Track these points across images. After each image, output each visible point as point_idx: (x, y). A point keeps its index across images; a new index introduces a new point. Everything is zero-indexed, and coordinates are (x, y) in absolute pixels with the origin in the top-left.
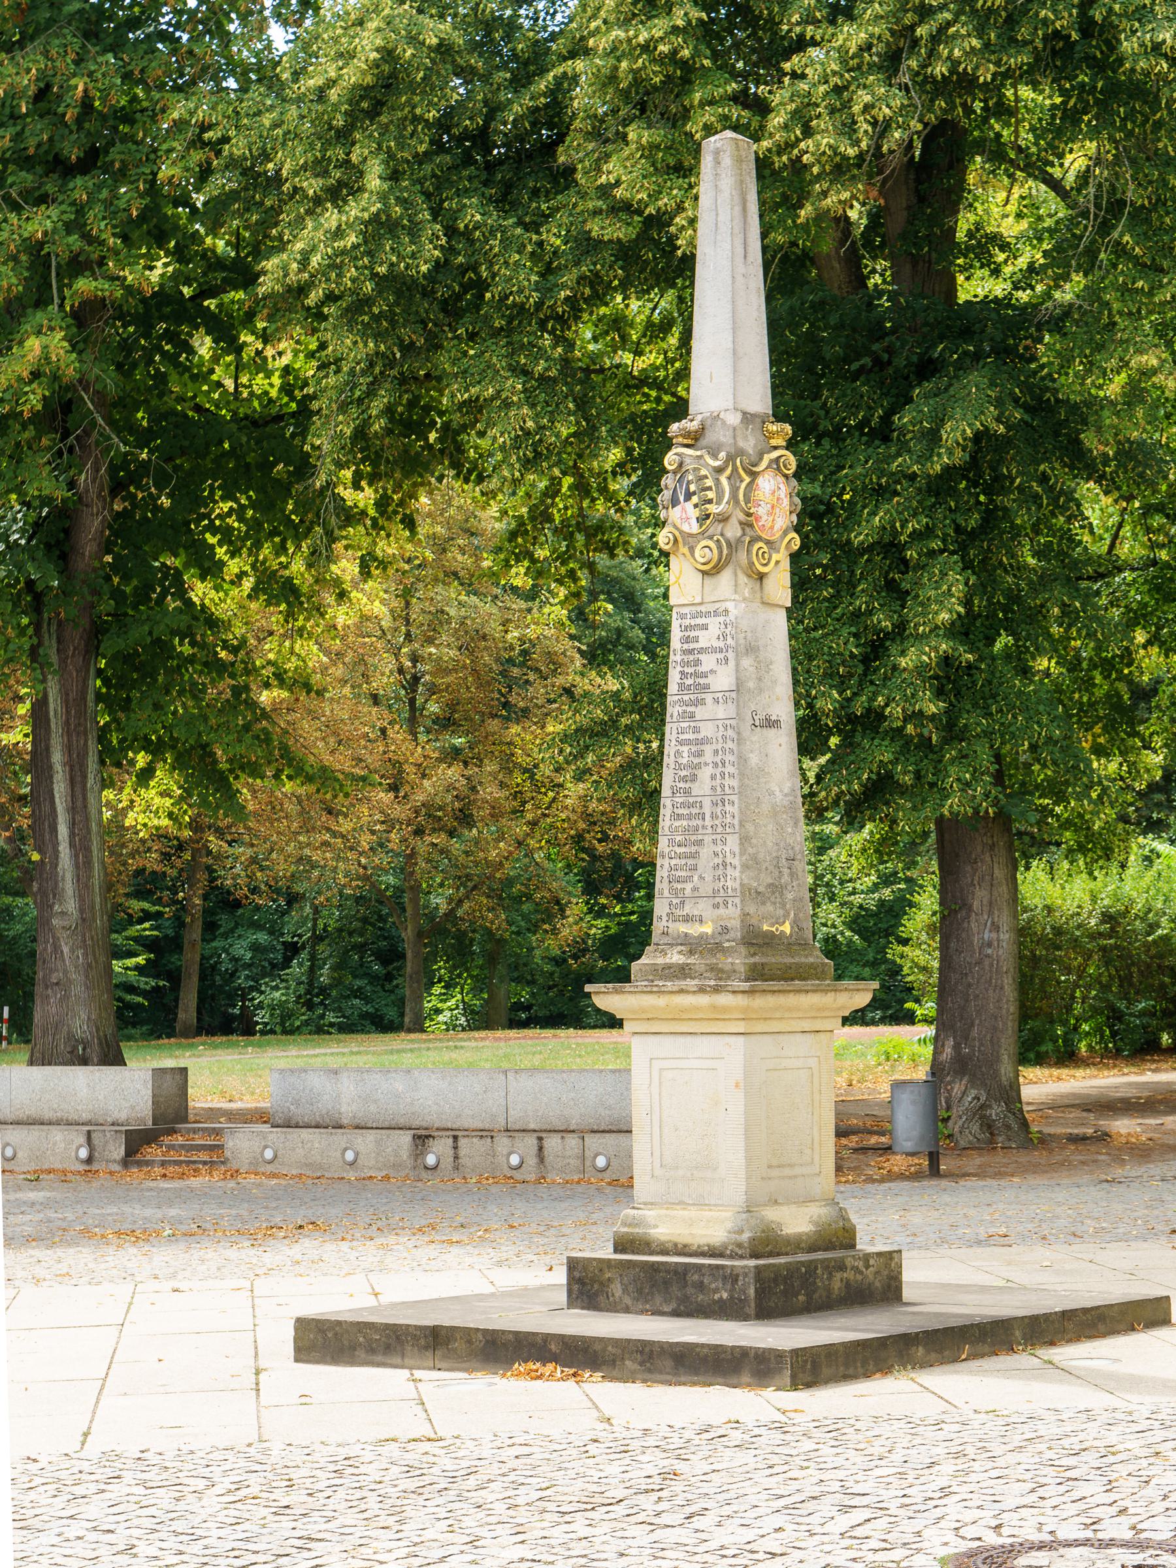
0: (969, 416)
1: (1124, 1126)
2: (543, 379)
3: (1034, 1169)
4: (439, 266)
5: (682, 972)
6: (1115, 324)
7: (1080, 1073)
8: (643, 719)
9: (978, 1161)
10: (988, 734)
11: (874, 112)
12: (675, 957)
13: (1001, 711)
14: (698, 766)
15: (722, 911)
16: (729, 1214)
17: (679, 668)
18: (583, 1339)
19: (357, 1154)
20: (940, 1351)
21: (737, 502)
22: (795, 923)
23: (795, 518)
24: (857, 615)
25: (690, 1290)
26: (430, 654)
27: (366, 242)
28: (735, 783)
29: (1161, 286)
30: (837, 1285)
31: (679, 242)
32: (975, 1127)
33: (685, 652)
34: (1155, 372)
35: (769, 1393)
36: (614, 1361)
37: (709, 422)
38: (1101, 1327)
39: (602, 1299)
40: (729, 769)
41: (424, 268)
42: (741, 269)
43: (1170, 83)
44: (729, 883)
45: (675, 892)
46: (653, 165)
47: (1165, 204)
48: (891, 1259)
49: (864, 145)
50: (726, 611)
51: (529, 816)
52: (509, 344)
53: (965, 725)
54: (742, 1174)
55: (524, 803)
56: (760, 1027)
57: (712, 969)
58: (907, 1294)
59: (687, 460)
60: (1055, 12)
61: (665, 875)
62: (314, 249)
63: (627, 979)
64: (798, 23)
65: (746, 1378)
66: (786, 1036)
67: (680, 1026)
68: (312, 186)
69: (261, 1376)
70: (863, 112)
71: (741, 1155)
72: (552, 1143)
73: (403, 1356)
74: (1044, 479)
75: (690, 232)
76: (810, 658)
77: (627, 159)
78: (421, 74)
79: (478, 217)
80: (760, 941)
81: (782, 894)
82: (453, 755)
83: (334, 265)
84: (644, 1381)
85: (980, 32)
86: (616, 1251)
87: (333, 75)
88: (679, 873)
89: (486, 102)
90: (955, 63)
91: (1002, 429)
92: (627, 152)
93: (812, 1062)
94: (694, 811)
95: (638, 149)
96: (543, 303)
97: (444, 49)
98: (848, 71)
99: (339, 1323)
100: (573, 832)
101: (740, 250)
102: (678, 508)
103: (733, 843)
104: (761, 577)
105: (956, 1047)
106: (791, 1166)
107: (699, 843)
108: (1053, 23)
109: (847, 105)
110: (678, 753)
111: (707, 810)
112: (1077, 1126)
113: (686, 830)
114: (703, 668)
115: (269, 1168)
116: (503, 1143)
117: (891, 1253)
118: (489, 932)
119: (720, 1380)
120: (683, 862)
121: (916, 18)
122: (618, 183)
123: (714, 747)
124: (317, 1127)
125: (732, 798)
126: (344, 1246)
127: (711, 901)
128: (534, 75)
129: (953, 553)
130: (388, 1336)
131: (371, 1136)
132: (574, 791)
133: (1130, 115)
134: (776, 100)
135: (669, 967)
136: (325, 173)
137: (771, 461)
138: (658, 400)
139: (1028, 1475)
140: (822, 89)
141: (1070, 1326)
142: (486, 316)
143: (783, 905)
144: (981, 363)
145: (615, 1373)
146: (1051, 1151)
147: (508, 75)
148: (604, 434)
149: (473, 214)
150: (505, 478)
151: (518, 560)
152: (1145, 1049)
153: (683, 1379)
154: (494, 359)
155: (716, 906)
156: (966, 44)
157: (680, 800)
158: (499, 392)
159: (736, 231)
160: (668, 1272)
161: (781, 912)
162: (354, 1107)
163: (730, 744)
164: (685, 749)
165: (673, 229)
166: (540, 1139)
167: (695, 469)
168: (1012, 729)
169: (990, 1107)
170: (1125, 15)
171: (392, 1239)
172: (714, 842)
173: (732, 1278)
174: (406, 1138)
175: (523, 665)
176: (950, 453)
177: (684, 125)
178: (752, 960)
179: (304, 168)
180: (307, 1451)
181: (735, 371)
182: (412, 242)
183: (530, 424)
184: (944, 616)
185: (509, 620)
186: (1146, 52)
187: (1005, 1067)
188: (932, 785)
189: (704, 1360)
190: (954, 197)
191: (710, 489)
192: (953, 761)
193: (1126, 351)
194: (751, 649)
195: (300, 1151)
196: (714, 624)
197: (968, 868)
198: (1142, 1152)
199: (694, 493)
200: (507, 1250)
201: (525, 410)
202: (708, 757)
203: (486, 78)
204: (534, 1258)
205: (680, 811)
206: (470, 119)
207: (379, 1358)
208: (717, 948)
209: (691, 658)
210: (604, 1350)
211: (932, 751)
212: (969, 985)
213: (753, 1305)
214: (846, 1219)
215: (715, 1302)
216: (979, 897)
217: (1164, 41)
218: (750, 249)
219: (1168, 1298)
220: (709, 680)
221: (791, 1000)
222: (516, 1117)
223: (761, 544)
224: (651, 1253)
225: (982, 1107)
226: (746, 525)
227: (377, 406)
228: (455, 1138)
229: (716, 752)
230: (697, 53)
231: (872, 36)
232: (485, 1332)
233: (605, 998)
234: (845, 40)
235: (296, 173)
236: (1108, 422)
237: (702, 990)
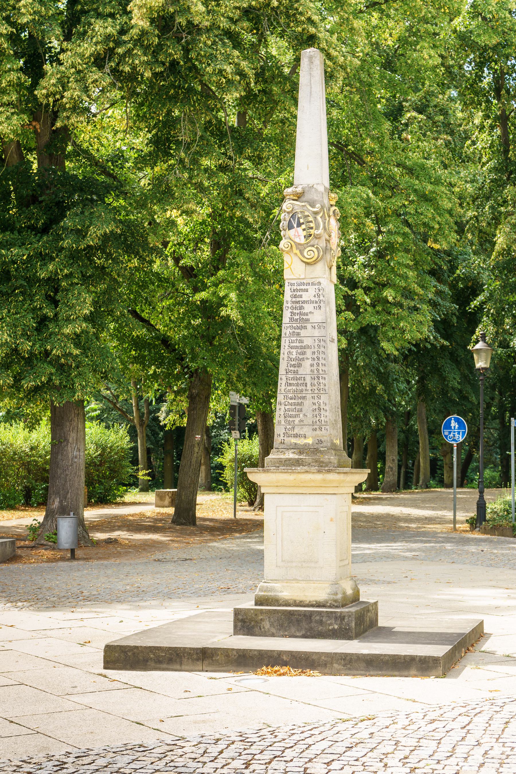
5: (298, 463)
12: (291, 455)
15: (318, 432)
16: (327, 585)
17: (290, 310)
24: (34, 309)
25: (313, 625)
37: (307, 189)
39: (257, 630)
44: (323, 418)
50: (319, 283)
57: (316, 461)
59: (296, 207)
61: (282, 413)
67: (299, 491)
73: (181, 664)
76: (16, 327)
86: (256, 604)
94: (300, 382)
102: (292, 231)
105: (61, 502)
107: (304, 398)
111: (308, 380)
119: (396, 673)
120: (293, 407)
123: (313, 350)
135: (290, 460)
153: (372, 673)
155: (315, 430)
160: (300, 615)
164: (294, 351)
167: (301, 212)
168: (97, 363)
172: (313, 398)
173: (341, 618)
191: (311, 222)
192: (76, 376)
196: (312, 290)
197: (68, 424)
199: (303, 223)
205: (291, 382)
207: (165, 666)
209: (298, 305)
212: (67, 475)
215: (329, 630)
220: (309, 316)
229: (314, 353)
232: (238, 650)
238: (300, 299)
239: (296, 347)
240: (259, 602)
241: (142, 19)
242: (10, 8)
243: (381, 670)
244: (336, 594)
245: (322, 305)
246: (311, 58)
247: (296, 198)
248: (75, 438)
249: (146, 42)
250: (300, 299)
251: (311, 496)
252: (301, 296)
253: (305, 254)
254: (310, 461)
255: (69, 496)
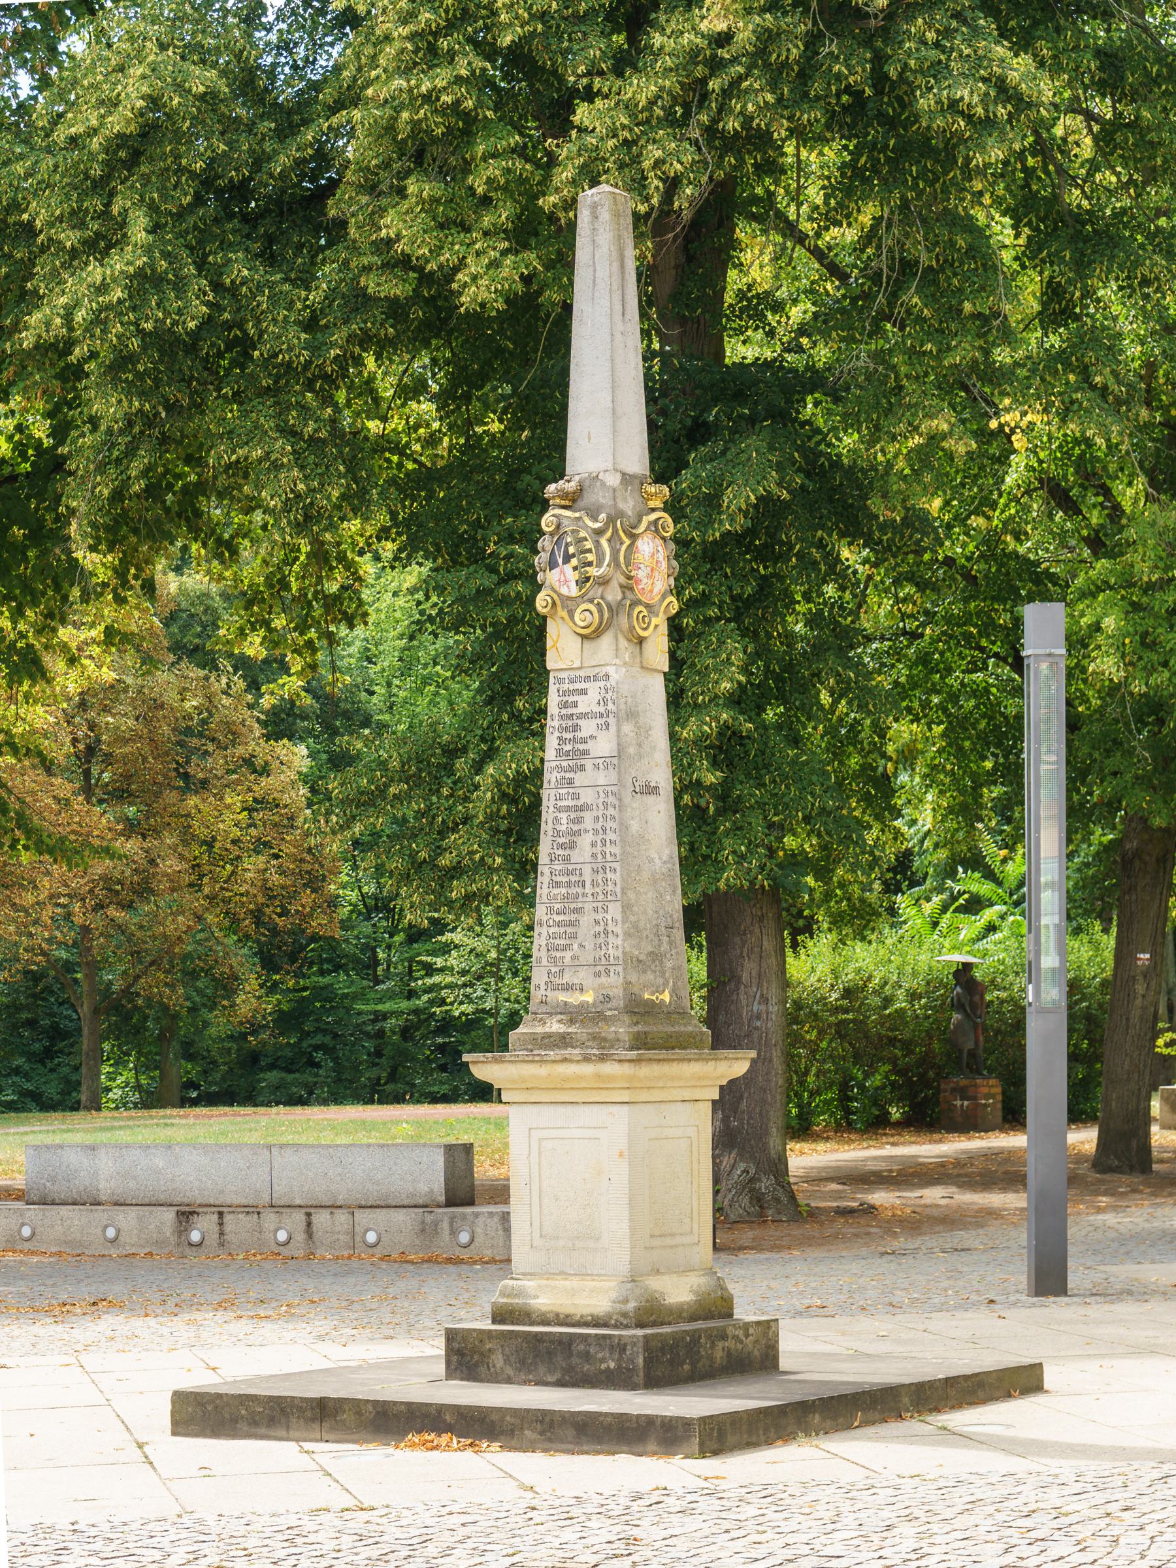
0: (752, 481)
1: (880, 1197)
2: (313, 440)
3: (806, 1242)
4: (207, 323)
5: (563, 1041)
6: (901, 388)
7: (821, 1146)
8: (410, 789)
9: (750, 1234)
10: (761, 805)
11: (666, 167)
12: (555, 1026)
13: (774, 781)
14: (578, 833)
15: (603, 979)
16: (613, 1284)
17: (557, 734)
18: (480, 1409)
19: (118, 1231)
20: (834, 1418)
21: (618, 565)
22: (674, 992)
23: (672, 582)
25: (575, 1360)
26: (107, 723)
27: (131, 297)
28: (616, 850)
29: (949, 349)
30: (719, 1354)
31: (463, 299)
32: (745, 1201)
33: (562, 717)
34: (944, 437)
35: (677, 1460)
36: (512, 1431)
37: (587, 483)
38: (981, 1394)
39: (482, 1369)
40: (611, 836)
41: (192, 325)
42: (619, 327)
43: (966, 141)
45: (554, 961)
46: (434, 219)
47: (952, 265)
48: (768, 1329)
49: (655, 201)
50: (607, 675)
51: (207, 891)
52: (276, 403)
53: (739, 796)
54: (626, 1243)
55: (201, 876)
56: (643, 1096)
57: (594, 1038)
58: (784, 1364)
59: (565, 522)
60: (848, 67)
61: (544, 943)
62: (77, 304)
63: (504, 1047)
64: (584, 75)
65: (652, 1447)
66: (667, 1106)
67: (562, 1096)
68: (70, 238)
69: (146, 1449)
70: (654, 168)
71: (625, 1225)
72: (321, 1219)
73: (288, 1428)
74: (821, 545)
75: (473, 288)
77: (407, 213)
78: (188, 123)
79: (246, 272)
80: (641, 1010)
81: (661, 962)
82: (131, 828)
83: (98, 321)
84: (545, 1451)
85: (773, 86)
86: (494, 1322)
87: (94, 122)
88: (558, 942)
89: (251, 151)
90: (747, 120)
91: (785, 495)
92: (405, 205)
93: (691, 1132)
94: (573, 878)
95: (418, 203)
96: (311, 362)
97: (209, 98)
98: (637, 125)
99: (219, 1396)
100: (252, 906)
101: (618, 307)
102: (556, 571)
103: (615, 911)
104: (641, 641)
106: (672, 1235)
107: (580, 911)
108: (847, 78)
109: (637, 160)
110: (557, 820)
111: (587, 877)
112: (835, 1200)
113: (565, 897)
114: (582, 734)
115: (27, 1246)
116: (270, 1219)
117: (768, 1322)
118: (166, 1008)
120: (562, 930)
121: (707, 72)
122: (399, 237)
123: (595, 813)
124: (74, 1204)
125: (614, 865)
126: (151, 1321)
127: (592, 970)
128: (299, 126)
129: (729, 621)
130: (272, 1409)
131: (133, 1212)
132: (252, 864)
133: (922, 175)
134: (564, 153)
135: (549, 1036)
136: (82, 225)
137: (650, 523)
138: (400, 466)
139: (994, 1536)
140: (611, 143)
141: (952, 1392)
142: (251, 375)
143: (663, 973)
144: (757, 427)
145: (513, 1443)
146: (822, 1224)
147: (273, 125)
148: (375, 497)
149: (240, 268)
150: (275, 541)
151: (254, 629)
152: (878, 1125)
153: (585, 1448)
154: (262, 419)
155: (598, 975)
156: (760, 99)
157: (559, 868)
158: (268, 454)
159: (615, 287)
161: (660, 981)
162: (113, 1184)
163: (611, 811)
164: (564, 816)
165: (455, 286)
166: (309, 1215)
167: (573, 531)
168: (786, 800)
169: (759, 1180)
170: (920, 71)
171: (197, 1316)
172: (595, 910)
173: (620, 1347)
174: (169, 1215)
175: (201, 735)
176: (732, 520)
177: (464, 179)
178: (636, 1029)
179: (60, 219)
180: (244, 1521)
181: (614, 431)
182: (178, 298)
183: (301, 487)
184: (726, 685)
185: (185, 689)
186: (942, 110)
187: (774, 1140)
188: (706, 857)
189: (608, 1429)
190: (724, 253)
191: (589, 551)
192: (727, 833)
193: (915, 415)
194: (632, 715)
195: (60, 1229)
196: (594, 691)
197: (737, 940)
198: (917, 1223)
199: (573, 556)
200: (323, 1325)
201: (296, 472)
202: (588, 823)
203: (250, 128)
204: (354, 1332)
205: (559, 879)
206: (236, 170)
207: (263, 1431)
208: (599, 1017)
209: (570, 723)
210: (502, 1420)
211: (705, 822)
213: (641, 1374)
214: (723, 1288)
215: (602, 1372)
216: (748, 969)
217: (962, 98)
218: (628, 307)
219: (1040, 1364)
220: (590, 745)
221: (675, 1069)
222: (281, 1192)
223: (641, 608)
224: (532, 1324)
225: (751, 1180)
226: (626, 588)
227: (135, 467)
228: (221, 1214)
229: (597, 819)
230: (480, 104)
231: (662, 89)
233: (484, 1068)
234: (634, 93)
235: (51, 225)
236: (895, 487)
237: (587, 1059)
238: (574, 711)
239: (567, 809)
240: (499, 1316)
241: (725, 17)
242: (484, 12)
243: (600, 1443)
244: (626, 1301)
245: (612, 720)
246: (594, 207)
247: (567, 503)
248: (754, 973)
249: (774, 56)
250: (574, 711)
251: (587, 1108)
252: (575, 705)
253: (577, 618)
254: (584, 1037)
255: (744, 1105)
